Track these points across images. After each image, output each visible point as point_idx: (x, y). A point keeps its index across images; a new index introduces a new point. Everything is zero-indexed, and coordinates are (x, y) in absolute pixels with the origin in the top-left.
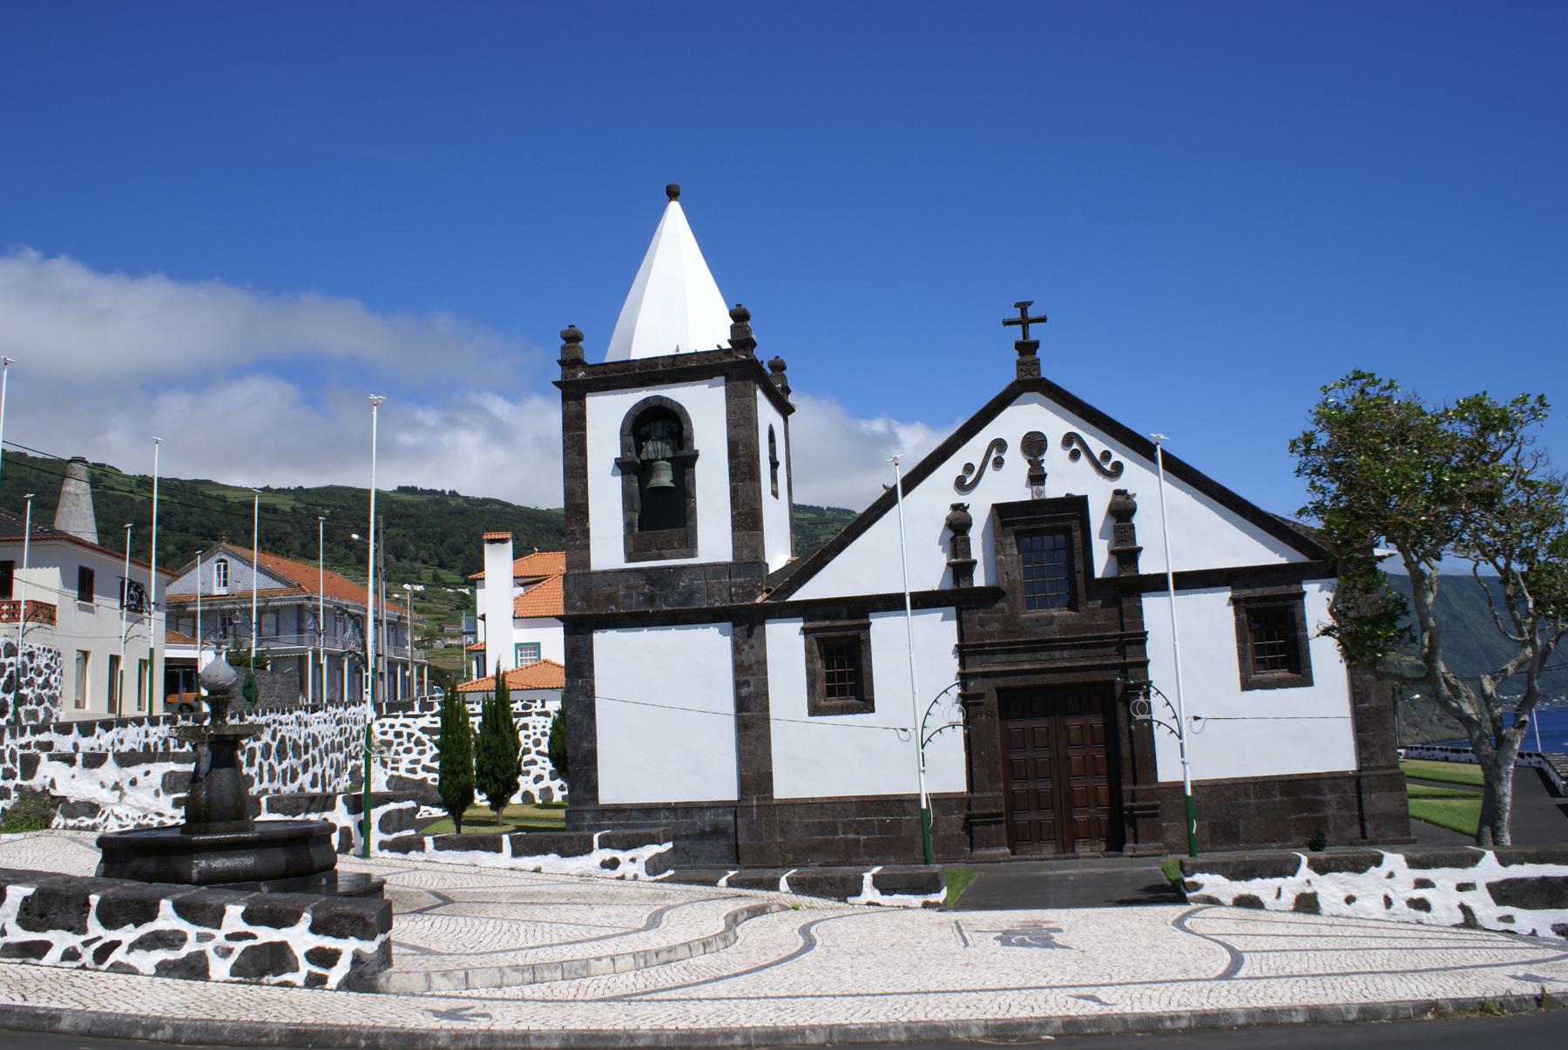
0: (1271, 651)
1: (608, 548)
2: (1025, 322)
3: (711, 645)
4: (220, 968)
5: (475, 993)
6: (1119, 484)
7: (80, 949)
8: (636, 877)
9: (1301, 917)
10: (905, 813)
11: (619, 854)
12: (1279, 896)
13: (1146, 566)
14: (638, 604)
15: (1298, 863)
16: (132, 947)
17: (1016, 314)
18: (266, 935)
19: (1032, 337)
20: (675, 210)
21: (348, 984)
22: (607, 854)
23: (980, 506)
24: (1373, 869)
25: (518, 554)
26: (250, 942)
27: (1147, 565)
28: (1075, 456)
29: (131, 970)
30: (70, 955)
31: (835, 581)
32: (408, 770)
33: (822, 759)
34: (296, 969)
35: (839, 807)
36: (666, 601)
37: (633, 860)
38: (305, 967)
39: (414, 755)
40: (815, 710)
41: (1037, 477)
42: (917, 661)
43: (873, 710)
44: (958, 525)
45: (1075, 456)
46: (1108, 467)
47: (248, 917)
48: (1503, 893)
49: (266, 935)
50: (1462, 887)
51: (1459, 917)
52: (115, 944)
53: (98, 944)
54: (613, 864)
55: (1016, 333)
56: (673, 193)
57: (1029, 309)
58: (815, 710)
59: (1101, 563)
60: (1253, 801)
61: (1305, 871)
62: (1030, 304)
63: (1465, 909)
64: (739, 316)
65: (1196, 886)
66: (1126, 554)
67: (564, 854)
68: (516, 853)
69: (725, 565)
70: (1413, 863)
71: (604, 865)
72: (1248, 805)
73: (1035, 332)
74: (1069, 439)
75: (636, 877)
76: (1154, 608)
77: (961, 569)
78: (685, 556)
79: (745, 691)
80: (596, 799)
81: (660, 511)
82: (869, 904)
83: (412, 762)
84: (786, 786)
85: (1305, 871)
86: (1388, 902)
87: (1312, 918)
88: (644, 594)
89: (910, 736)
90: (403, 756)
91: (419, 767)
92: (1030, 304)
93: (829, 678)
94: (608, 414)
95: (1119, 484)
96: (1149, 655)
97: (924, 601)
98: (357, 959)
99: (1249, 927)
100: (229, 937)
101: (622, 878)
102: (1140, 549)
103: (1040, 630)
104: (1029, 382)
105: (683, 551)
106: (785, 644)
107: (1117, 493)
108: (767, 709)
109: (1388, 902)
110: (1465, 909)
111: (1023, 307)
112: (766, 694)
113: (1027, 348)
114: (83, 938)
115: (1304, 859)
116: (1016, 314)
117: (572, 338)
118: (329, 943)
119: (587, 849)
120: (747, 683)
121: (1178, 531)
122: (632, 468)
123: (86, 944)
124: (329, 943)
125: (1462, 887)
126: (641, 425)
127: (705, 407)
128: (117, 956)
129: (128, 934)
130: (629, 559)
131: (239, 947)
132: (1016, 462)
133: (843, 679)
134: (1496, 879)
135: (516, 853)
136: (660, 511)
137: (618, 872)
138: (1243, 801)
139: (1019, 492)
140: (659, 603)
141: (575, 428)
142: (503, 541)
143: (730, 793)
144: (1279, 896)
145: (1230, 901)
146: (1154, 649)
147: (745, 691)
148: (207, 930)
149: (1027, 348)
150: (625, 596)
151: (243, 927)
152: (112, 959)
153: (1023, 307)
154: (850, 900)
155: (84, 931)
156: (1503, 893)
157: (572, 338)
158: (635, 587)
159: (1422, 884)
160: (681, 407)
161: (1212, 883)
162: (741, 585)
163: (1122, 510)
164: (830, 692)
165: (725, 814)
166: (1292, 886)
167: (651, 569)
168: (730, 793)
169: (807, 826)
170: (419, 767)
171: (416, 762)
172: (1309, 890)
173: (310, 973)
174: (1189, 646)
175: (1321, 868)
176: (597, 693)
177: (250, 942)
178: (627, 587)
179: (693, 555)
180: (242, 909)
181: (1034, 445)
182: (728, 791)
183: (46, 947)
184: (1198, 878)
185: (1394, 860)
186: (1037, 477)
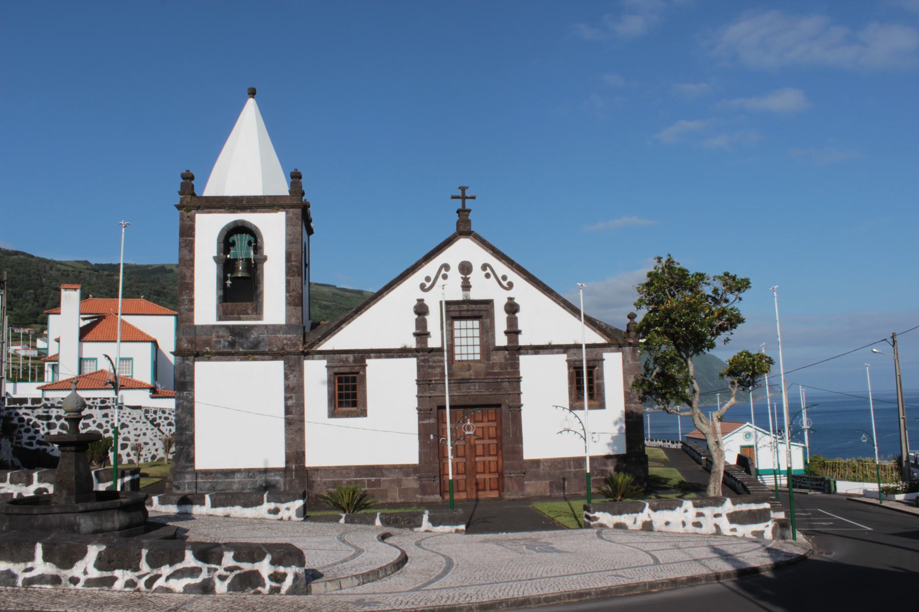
0: (585, 386)
1: (206, 309)
2: (464, 198)
3: (273, 371)
4: (221, 587)
5: (344, 591)
6: (510, 294)
7: (136, 580)
8: (290, 518)
9: (644, 533)
10: (383, 475)
11: (279, 505)
12: (635, 522)
13: (523, 341)
14: (224, 347)
15: (644, 506)
16: (168, 578)
17: (459, 193)
18: (247, 566)
19: (467, 207)
20: (251, 105)
21: (293, 591)
22: (272, 505)
23: (433, 301)
24: (678, 508)
25: (84, 297)
26: (238, 572)
27: (523, 341)
28: (488, 276)
29: (168, 590)
30: (130, 584)
31: (346, 338)
32: (26, 444)
33: (335, 444)
34: (264, 586)
35: (344, 472)
36: (242, 346)
37: (288, 509)
38: (269, 584)
39: (32, 434)
40: (332, 414)
41: (466, 286)
42: (393, 388)
43: (366, 416)
44: (421, 310)
45: (488, 276)
46: (505, 283)
47: (236, 558)
48: (734, 518)
49: (247, 566)
50: (716, 516)
51: (714, 530)
52: (158, 576)
53: (147, 578)
54: (276, 511)
55: (458, 204)
56: (252, 93)
57: (466, 191)
58: (332, 414)
59: (501, 340)
60: (573, 470)
61: (647, 510)
62: (467, 188)
63: (717, 526)
64: (295, 178)
65: (595, 519)
66: (513, 332)
67: (245, 505)
68: (214, 505)
69: (281, 326)
70: (695, 506)
71: (270, 512)
72: (570, 472)
73: (469, 204)
74: (485, 267)
75: (290, 518)
76: (526, 362)
77: (422, 334)
78: (255, 319)
79: (290, 402)
80: (194, 466)
81: (240, 287)
82: (426, 531)
83: (30, 438)
84: (311, 461)
85: (647, 510)
86: (684, 524)
87: (651, 533)
88: (228, 342)
89: (387, 432)
90: (24, 434)
91: (34, 442)
92: (467, 188)
93: (340, 396)
94: (209, 228)
95: (510, 294)
96: (522, 390)
97: (403, 353)
98: (296, 577)
99: (647, 539)
100: (226, 569)
101: (281, 519)
102: (265, 259)
103: (463, 373)
104: (464, 230)
105: (254, 316)
106: (316, 373)
107: (511, 299)
108: (303, 414)
109: (684, 524)
110: (717, 526)
111: (463, 189)
112: (303, 405)
113: (463, 213)
114: (137, 574)
115: (647, 504)
116: (459, 193)
117: (188, 178)
118: (281, 569)
119: (259, 503)
120: (290, 398)
121: (543, 321)
122: (226, 266)
123: (140, 577)
124: (281, 569)
125: (716, 516)
126: (228, 238)
127: (273, 229)
128: (160, 582)
129: (166, 570)
130: (220, 318)
131: (232, 575)
132: (455, 276)
133: (348, 394)
134: (731, 511)
135: (214, 505)
136: (240, 287)
137: (280, 515)
138: (568, 470)
139: (457, 295)
140: (241, 345)
141: (187, 233)
142: (75, 289)
143: (280, 463)
144: (635, 522)
145: (611, 526)
146: (525, 386)
147: (290, 402)
148: (213, 566)
149: (463, 213)
150: (216, 342)
151: (232, 563)
152: (155, 585)
153: (463, 189)
154: (416, 529)
155: (137, 569)
156: (734, 518)
157: (188, 178)
158: (223, 337)
159: (700, 515)
160: (256, 228)
161: (605, 518)
162: (290, 339)
163: (512, 308)
164: (341, 404)
165: (275, 476)
166: (642, 517)
167: (233, 326)
168: (280, 463)
169: (325, 483)
170: (34, 442)
171: (33, 438)
172: (648, 520)
173: (271, 587)
174: (542, 385)
175: (655, 509)
176: (196, 400)
177: (238, 572)
178: (218, 337)
179: (260, 319)
180: (232, 554)
181: (465, 268)
182: (278, 461)
183: (115, 579)
184: (597, 514)
185: (688, 504)
186: (466, 286)
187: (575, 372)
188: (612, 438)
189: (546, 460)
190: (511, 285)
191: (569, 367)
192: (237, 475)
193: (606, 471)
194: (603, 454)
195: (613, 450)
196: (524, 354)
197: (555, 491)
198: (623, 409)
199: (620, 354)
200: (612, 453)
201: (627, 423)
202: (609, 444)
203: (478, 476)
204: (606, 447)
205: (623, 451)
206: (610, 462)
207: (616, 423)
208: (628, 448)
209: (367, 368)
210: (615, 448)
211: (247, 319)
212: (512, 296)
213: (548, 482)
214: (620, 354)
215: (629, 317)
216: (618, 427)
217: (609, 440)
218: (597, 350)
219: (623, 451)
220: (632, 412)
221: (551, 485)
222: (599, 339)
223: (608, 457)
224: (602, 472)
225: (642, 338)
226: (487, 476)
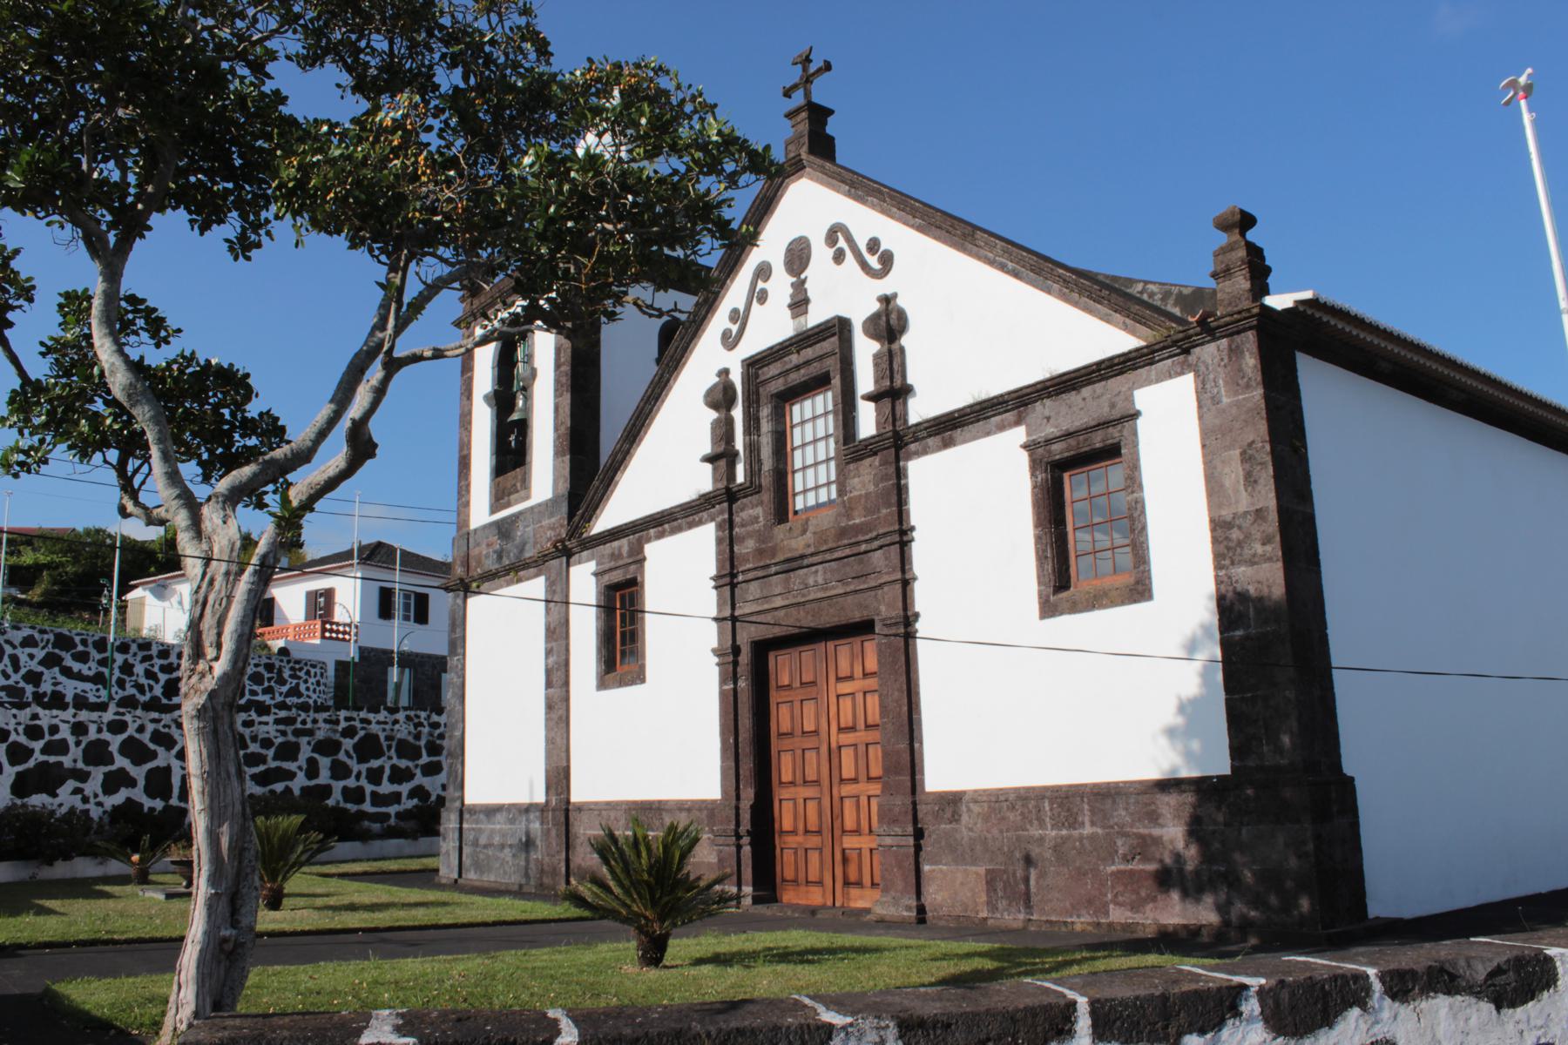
6: (885, 286)
13: (919, 410)
72: (1041, 839)
73: (822, 92)
103: (793, 544)
187: (1055, 474)
188: (1182, 708)
189: (980, 797)
190: (887, 260)
191: (1035, 465)
192: (499, 817)
193: (1157, 841)
194: (1153, 773)
195: (1188, 755)
196: (918, 454)
197: (1002, 904)
198: (1211, 587)
199: (1188, 380)
200: (1184, 773)
201: (1226, 645)
202: (1171, 732)
203: (849, 842)
204: (1163, 741)
205: (1220, 764)
206: (1168, 801)
207: (1192, 647)
208: (1238, 751)
209: (647, 564)
210: (1195, 745)
211: (517, 502)
212: (889, 292)
213: (982, 870)
214: (1188, 380)
215: (1223, 225)
216: (1197, 666)
217: (1170, 717)
218: (1115, 384)
219: (1220, 764)
220: (1242, 597)
221: (991, 880)
222: (1101, 338)
223: (1167, 785)
224: (1144, 846)
225: (71, 119)
226: (865, 843)
